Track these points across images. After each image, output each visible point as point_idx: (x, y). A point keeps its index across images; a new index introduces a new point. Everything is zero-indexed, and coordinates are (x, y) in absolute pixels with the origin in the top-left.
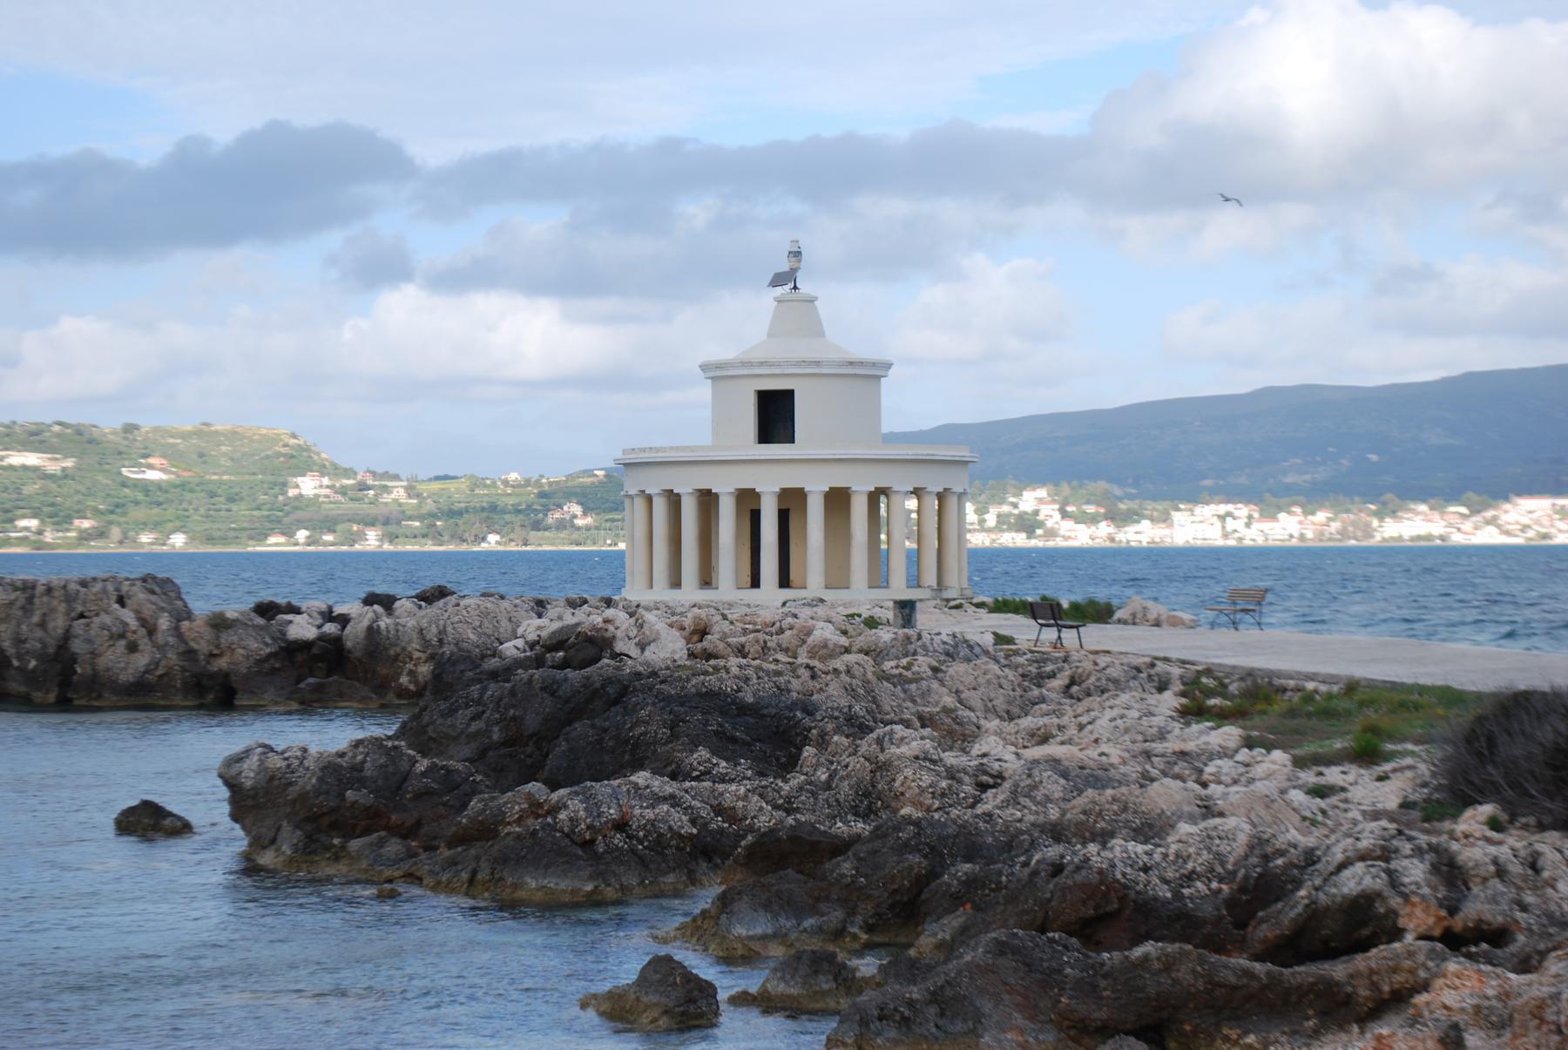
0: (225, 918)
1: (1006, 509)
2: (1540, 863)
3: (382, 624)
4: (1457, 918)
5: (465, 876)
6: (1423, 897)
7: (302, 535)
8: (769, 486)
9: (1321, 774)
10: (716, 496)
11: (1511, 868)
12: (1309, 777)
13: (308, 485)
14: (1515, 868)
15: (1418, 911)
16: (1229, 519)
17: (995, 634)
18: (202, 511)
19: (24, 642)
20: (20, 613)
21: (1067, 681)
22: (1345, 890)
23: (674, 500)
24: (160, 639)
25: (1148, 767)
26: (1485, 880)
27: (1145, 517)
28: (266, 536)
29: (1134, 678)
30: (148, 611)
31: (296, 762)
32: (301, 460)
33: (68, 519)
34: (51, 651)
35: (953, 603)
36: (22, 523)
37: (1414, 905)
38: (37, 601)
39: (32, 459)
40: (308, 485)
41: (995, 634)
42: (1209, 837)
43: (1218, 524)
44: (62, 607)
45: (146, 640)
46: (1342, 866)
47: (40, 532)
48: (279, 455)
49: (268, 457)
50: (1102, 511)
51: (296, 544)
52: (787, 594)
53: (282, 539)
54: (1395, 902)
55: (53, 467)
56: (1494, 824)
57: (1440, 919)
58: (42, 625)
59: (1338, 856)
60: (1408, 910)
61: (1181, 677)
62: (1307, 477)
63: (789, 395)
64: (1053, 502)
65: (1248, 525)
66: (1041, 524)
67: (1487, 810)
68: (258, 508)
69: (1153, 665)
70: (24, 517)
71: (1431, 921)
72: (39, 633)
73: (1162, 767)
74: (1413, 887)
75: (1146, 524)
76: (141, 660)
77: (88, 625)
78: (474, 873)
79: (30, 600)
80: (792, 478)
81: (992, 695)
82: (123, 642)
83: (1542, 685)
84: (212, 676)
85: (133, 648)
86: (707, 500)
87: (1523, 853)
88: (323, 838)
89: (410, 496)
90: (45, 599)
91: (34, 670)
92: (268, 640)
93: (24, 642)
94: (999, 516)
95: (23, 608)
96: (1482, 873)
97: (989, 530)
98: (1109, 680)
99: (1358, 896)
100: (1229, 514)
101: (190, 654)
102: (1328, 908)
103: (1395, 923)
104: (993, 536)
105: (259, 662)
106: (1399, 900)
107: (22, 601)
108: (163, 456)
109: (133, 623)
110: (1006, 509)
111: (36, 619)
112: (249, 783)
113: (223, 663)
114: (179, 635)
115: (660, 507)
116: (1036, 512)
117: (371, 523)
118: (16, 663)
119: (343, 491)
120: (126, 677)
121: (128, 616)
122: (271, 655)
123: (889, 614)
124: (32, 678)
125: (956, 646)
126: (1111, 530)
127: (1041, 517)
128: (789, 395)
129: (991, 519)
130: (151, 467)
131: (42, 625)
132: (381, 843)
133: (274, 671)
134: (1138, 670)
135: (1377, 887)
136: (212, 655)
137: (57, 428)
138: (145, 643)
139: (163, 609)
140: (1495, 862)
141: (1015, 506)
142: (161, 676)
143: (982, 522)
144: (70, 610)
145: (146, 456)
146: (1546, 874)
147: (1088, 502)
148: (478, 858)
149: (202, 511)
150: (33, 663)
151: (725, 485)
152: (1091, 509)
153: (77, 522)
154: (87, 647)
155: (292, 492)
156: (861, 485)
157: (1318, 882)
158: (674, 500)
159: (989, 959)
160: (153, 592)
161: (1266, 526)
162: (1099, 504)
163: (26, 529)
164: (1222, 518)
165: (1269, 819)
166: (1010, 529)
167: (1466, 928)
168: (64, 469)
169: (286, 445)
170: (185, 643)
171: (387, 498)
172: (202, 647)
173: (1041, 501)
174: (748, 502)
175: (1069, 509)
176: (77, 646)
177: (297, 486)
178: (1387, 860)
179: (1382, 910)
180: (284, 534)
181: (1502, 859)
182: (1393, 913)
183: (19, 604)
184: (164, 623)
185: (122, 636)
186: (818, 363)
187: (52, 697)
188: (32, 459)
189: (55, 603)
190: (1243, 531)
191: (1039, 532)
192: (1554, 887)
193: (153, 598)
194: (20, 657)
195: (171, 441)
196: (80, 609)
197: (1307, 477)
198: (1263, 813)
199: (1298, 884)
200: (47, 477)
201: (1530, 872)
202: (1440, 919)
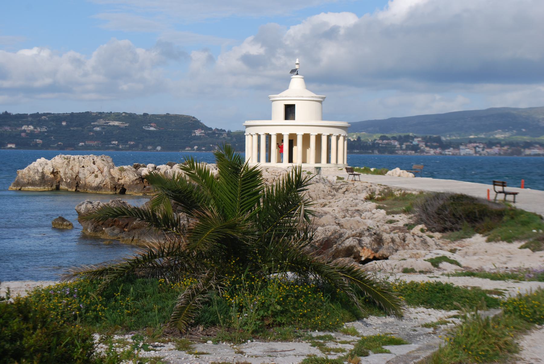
1: (409, 143)
2: (406, 239)
3: (168, 171)
5: (131, 238)
6: (367, 248)
7: (196, 147)
8: (286, 132)
9: (393, 217)
10: (271, 135)
12: (390, 217)
13: (198, 133)
14: (398, 240)
15: (366, 251)
16: (477, 148)
17: (338, 177)
22: (346, 245)
23: (259, 136)
24: (104, 174)
26: (388, 243)
30: (101, 166)
32: (195, 124)
33: (127, 142)
36: (114, 142)
39: (116, 123)
40: (198, 133)
41: (338, 177)
42: (326, 231)
43: (474, 150)
44: (78, 164)
46: (347, 238)
47: (118, 145)
51: (194, 150)
53: (190, 149)
54: (359, 248)
56: (422, 230)
57: (372, 254)
58: (72, 169)
59: (347, 236)
62: (503, 136)
64: (423, 142)
65: (483, 150)
66: (419, 148)
67: (421, 226)
68: (183, 139)
69: (371, 186)
70: (113, 141)
71: (370, 254)
72: (71, 171)
75: (452, 149)
76: (98, 180)
78: (133, 237)
79: (69, 162)
80: (293, 130)
83: (445, 192)
85: (96, 176)
86: (268, 137)
87: (401, 236)
88: (100, 228)
89: (228, 137)
94: (406, 146)
96: (388, 241)
100: (477, 146)
101: (113, 178)
102: (341, 250)
103: (359, 254)
105: (133, 181)
106: (360, 248)
107: (66, 162)
108: (155, 123)
109: (97, 170)
110: (409, 143)
111: (70, 167)
113: (122, 182)
114: (110, 174)
115: (255, 138)
116: (418, 145)
120: (95, 185)
121: (95, 167)
122: (136, 179)
124: (68, 184)
125: (320, 180)
126: (440, 151)
127: (419, 146)
129: (404, 146)
130: (151, 126)
131: (72, 169)
132: (114, 230)
133: (137, 184)
134: (367, 187)
136: (119, 179)
137: (124, 114)
138: (100, 175)
139: (105, 165)
140: (392, 238)
141: (412, 143)
145: (150, 123)
146: (406, 242)
147: (434, 142)
148: (135, 233)
150: (69, 180)
151: (273, 132)
152: (435, 144)
153: (129, 142)
155: (193, 135)
156: (325, 132)
157: (340, 243)
158: (268, 137)
160: (103, 160)
161: (488, 150)
162: (437, 143)
163: (114, 144)
164: (475, 148)
165: (357, 227)
166: (410, 150)
167: (379, 257)
171: (221, 137)
172: (32, 176)
173: (419, 141)
174: (280, 137)
175: (428, 144)
176: (81, 176)
178: (361, 237)
181: (394, 237)
182: (359, 252)
183: (65, 163)
184: (106, 169)
185: (93, 173)
186: (302, 97)
187: (74, 190)
188: (116, 123)
190: (482, 152)
191: (419, 151)
193: (103, 162)
197: (503, 136)
199: (336, 243)
202: (372, 254)
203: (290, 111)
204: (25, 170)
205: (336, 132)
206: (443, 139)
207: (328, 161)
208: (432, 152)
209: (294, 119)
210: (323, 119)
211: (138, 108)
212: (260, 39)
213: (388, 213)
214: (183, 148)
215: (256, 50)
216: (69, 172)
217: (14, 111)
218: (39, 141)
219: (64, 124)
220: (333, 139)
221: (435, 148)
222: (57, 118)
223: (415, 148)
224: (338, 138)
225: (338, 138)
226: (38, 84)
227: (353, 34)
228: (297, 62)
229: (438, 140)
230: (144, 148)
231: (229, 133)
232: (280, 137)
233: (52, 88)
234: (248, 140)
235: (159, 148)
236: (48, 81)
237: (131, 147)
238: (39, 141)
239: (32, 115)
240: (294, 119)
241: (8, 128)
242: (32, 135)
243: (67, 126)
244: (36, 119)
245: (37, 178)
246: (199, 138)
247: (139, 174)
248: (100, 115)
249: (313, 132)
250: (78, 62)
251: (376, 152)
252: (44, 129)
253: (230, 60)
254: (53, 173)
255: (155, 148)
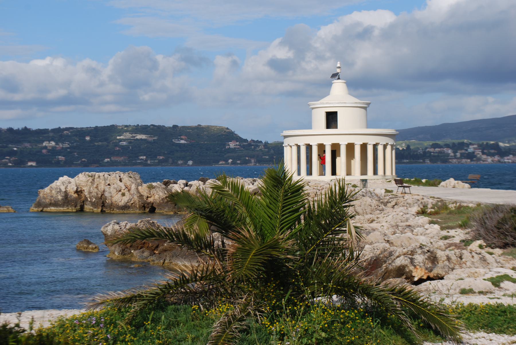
0: (159, 291)
1: (463, 151)
3: (201, 187)
4: (432, 273)
8: (328, 142)
9: (448, 232)
10: (311, 146)
11: (452, 258)
13: (232, 145)
14: (454, 258)
17: (386, 189)
18: (198, 153)
19: (92, 193)
20: (90, 184)
21: (394, 204)
22: (397, 264)
23: (299, 147)
25: (396, 230)
26: (444, 261)
27: (511, 154)
28: (219, 162)
29: (416, 203)
30: (128, 183)
31: (123, 227)
32: (230, 135)
34: (100, 196)
35: (388, 180)
36: (141, 157)
37: (417, 269)
38: (95, 180)
39: (143, 137)
40: (232, 145)
41: (386, 189)
42: (374, 249)
44: (103, 182)
45: (128, 192)
46: (398, 257)
47: (146, 160)
48: (223, 135)
49: (219, 136)
50: (496, 152)
51: (228, 164)
52: (334, 177)
53: (224, 163)
54: (412, 268)
55: (151, 139)
56: (481, 247)
60: (415, 270)
61: (432, 203)
63: (335, 113)
64: (479, 149)
66: (475, 156)
67: (479, 242)
68: (216, 152)
69: (423, 199)
70: (141, 156)
71: (423, 273)
72: (96, 190)
73: (401, 230)
74: (418, 263)
75: (511, 156)
76: (125, 199)
77: (110, 188)
78: (165, 260)
79: (93, 180)
81: (366, 208)
82: (121, 193)
84: (148, 204)
85: (123, 195)
86: (309, 147)
89: (265, 148)
90: (98, 179)
91: (94, 202)
92: (166, 192)
93: (92, 193)
94: (461, 154)
95: (91, 182)
97: (458, 158)
98: (407, 203)
99: (400, 266)
101: (141, 196)
102: (391, 270)
104: (459, 161)
106: (413, 267)
108: (186, 136)
109: (124, 187)
110: (463, 151)
111: (95, 186)
112: (109, 234)
113: (151, 200)
114: (138, 192)
115: (295, 149)
117: (252, 157)
118: (89, 200)
119: (244, 147)
120: (122, 203)
123: (359, 184)
124: (94, 204)
128: (335, 113)
129: (458, 155)
130: (182, 139)
134: (418, 200)
135: (406, 263)
136: (148, 197)
138: (127, 193)
139: (133, 183)
141: (467, 150)
142: (132, 204)
143: (455, 156)
144: (105, 183)
145: (180, 136)
146: (463, 260)
148: (166, 256)
149: (198, 153)
150: (94, 199)
151: (314, 142)
152: (492, 151)
153: (158, 157)
154: (110, 195)
155: (227, 147)
156: (371, 141)
157: (390, 262)
158: (309, 147)
159: (121, 257)
160: (131, 177)
162: (495, 150)
163: (142, 159)
165: (408, 245)
166: (465, 158)
168: (154, 140)
169: (225, 132)
170: (140, 193)
171: (258, 149)
172: (145, 193)
176: (107, 194)
177: (229, 145)
178: (413, 255)
179: (408, 270)
180: (224, 161)
182: (411, 271)
183: (90, 181)
184: (133, 187)
185: (120, 191)
188: (143, 137)
189: (101, 181)
192: (465, 264)
193: (130, 179)
194: (90, 198)
195: (188, 131)
196: (108, 183)
198: (406, 243)
199: (385, 262)
200: (150, 143)
201: (459, 259)
203: (331, 119)
204: (47, 190)
205: (383, 140)
206: (501, 144)
207: (375, 172)
208: (490, 160)
209: (336, 127)
210: (368, 127)
211: (167, 119)
212: (289, 42)
213: (442, 229)
214: (217, 162)
215: (283, 53)
216: (94, 191)
217: (34, 126)
218: (61, 158)
219: (88, 138)
220: (380, 148)
221: (492, 155)
222: (80, 133)
223: (471, 156)
224: (385, 147)
225: (385, 147)
226: (51, 96)
227: (388, 34)
228: (338, 65)
229: (496, 147)
230: (175, 163)
231: (266, 144)
232: (321, 148)
233: (67, 101)
234: (287, 152)
235: (190, 163)
236: (62, 92)
237: (160, 162)
238: (61, 158)
239: (54, 131)
240: (336, 127)
241: (27, 145)
242: (54, 152)
243: (91, 141)
244: (58, 134)
245: (60, 198)
246: (233, 150)
247: (169, 191)
248: (126, 128)
249: (358, 142)
250: (93, 71)
251: (428, 161)
252: (66, 145)
253: (256, 65)
254: (77, 192)
255: (186, 163)
